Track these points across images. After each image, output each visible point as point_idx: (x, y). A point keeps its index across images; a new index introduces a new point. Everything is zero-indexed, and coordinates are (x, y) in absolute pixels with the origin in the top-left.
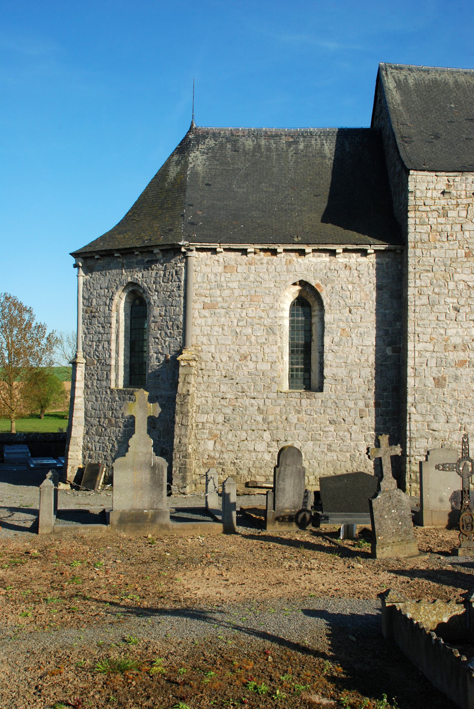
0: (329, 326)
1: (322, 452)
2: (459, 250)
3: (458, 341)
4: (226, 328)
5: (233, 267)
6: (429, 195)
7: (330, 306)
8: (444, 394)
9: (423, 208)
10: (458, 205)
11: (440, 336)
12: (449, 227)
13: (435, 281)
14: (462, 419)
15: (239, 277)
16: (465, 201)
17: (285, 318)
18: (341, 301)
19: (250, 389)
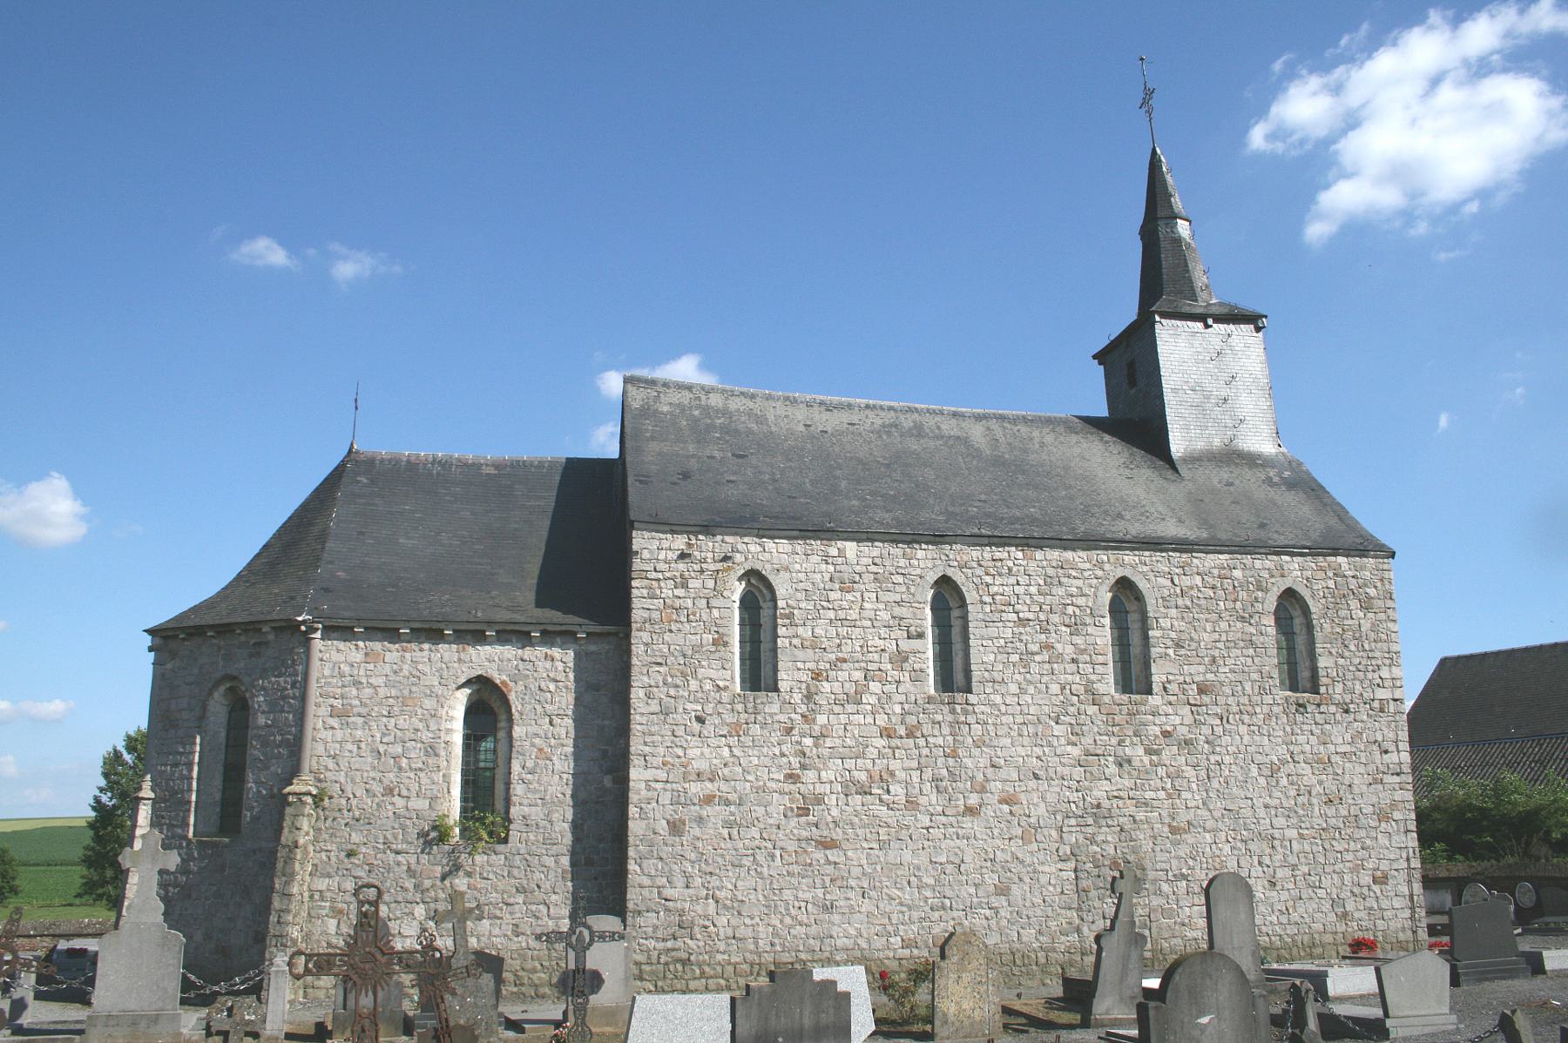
0: (519, 743)
1: (505, 935)
2: (704, 636)
3: (701, 765)
4: (363, 745)
5: (379, 654)
6: (662, 556)
7: (522, 714)
8: (682, 845)
9: (654, 575)
10: (702, 571)
11: (677, 760)
12: (689, 603)
13: (670, 680)
14: (709, 882)
15: (387, 669)
16: (712, 567)
17: (456, 731)
18: (538, 707)
19: (396, 839)
